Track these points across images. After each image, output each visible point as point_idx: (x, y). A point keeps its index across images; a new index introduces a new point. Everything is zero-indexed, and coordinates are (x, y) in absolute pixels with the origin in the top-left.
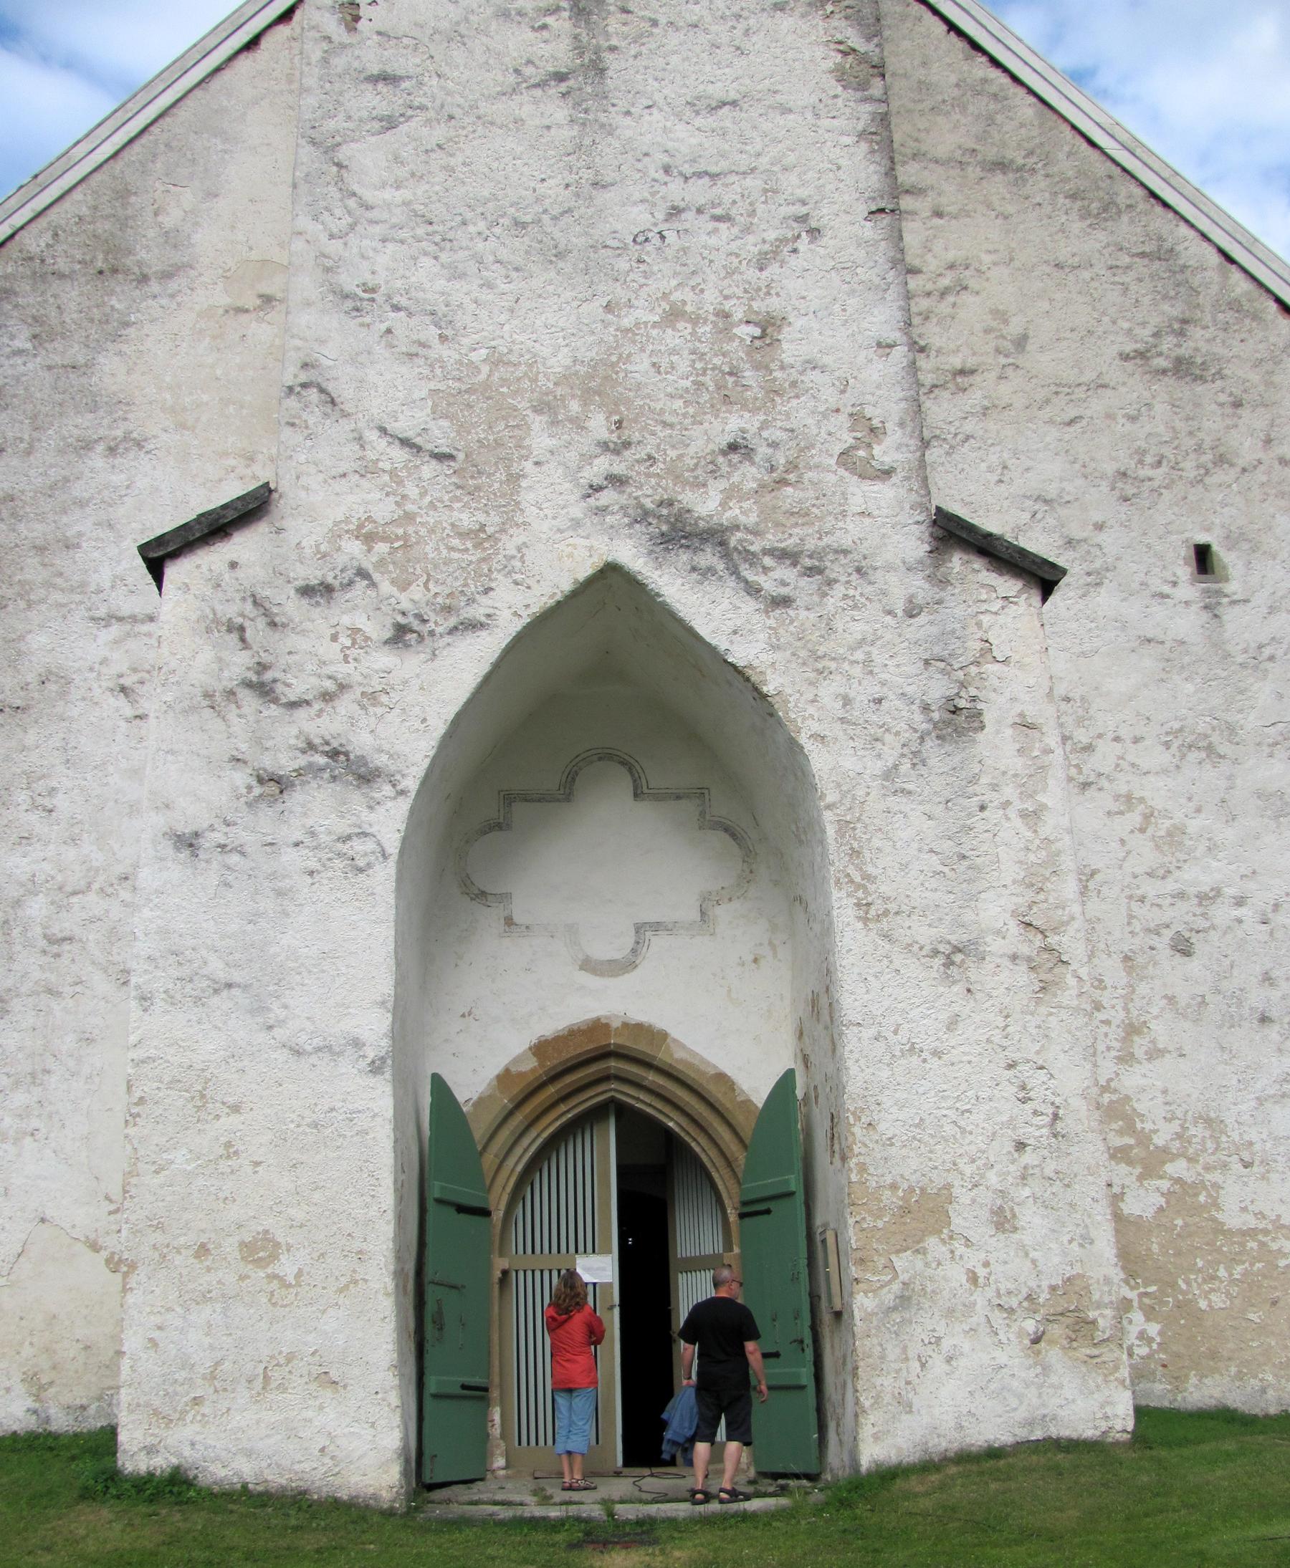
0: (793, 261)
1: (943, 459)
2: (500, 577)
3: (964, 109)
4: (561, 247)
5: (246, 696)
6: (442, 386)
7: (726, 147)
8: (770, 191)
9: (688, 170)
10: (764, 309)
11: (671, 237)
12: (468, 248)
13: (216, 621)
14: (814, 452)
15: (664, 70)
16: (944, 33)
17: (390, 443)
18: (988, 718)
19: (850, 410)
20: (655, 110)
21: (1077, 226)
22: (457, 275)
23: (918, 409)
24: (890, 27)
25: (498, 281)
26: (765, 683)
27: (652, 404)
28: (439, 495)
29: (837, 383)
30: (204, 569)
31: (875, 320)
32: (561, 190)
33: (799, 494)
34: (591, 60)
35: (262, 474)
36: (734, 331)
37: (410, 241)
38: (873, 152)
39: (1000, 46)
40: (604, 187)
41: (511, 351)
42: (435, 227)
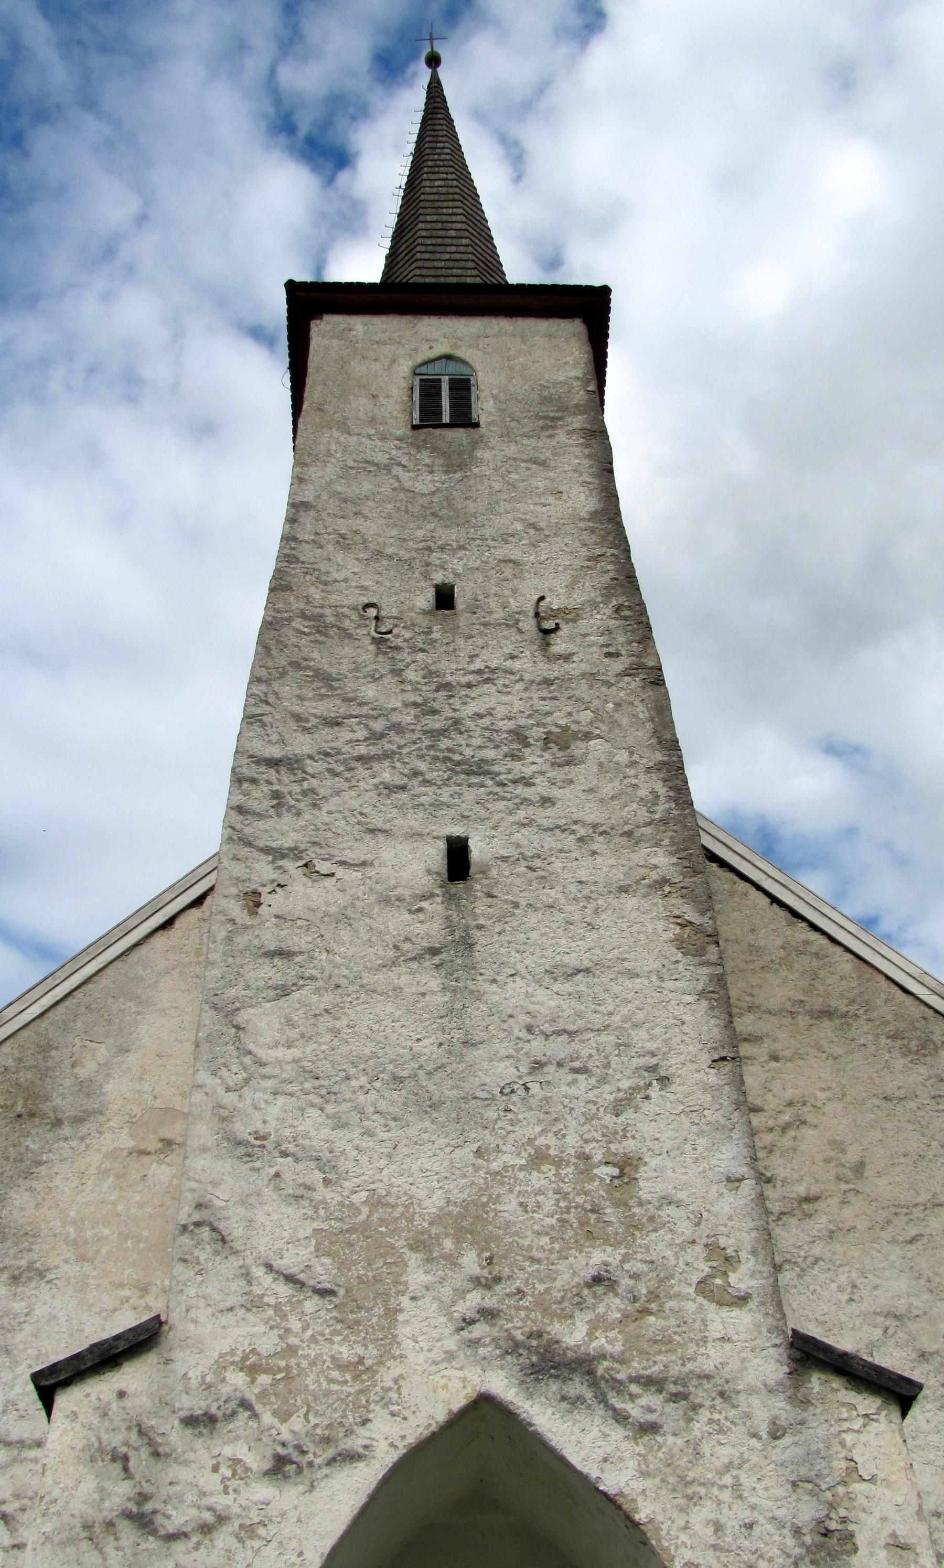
0: (646, 1107)
1: (795, 1282)
2: (377, 1408)
3: (790, 967)
4: (435, 1099)
5: (124, 1527)
6: (322, 1226)
7: (582, 1008)
8: (623, 1046)
9: (547, 1028)
10: (621, 1151)
11: (535, 1088)
12: (350, 1100)
13: (101, 1450)
14: (673, 1281)
15: (525, 944)
16: (768, 905)
17: (275, 1280)
18: (861, 1539)
19: (704, 1241)
20: (517, 978)
21: (900, 1063)
22: (340, 1124)
23: (768, 1237)
24: (720, 902)
25: (378, 1130)
26: (636, 1510)
27: (520, 1241)
28: (320, 1328)
29: (692, 1216)
30: (93, 1397)
31: (723, 1157)
32: (434, 1048)
33: (661, 1323)
34: (461, 937)
35: (155, 1305)
36: (595, 1171)
37: (298, 1094)
38: (712, 1008)
39: (817, 913)
40: (473, 1045)
41: (389, 1194)
42: (322, 1082)
